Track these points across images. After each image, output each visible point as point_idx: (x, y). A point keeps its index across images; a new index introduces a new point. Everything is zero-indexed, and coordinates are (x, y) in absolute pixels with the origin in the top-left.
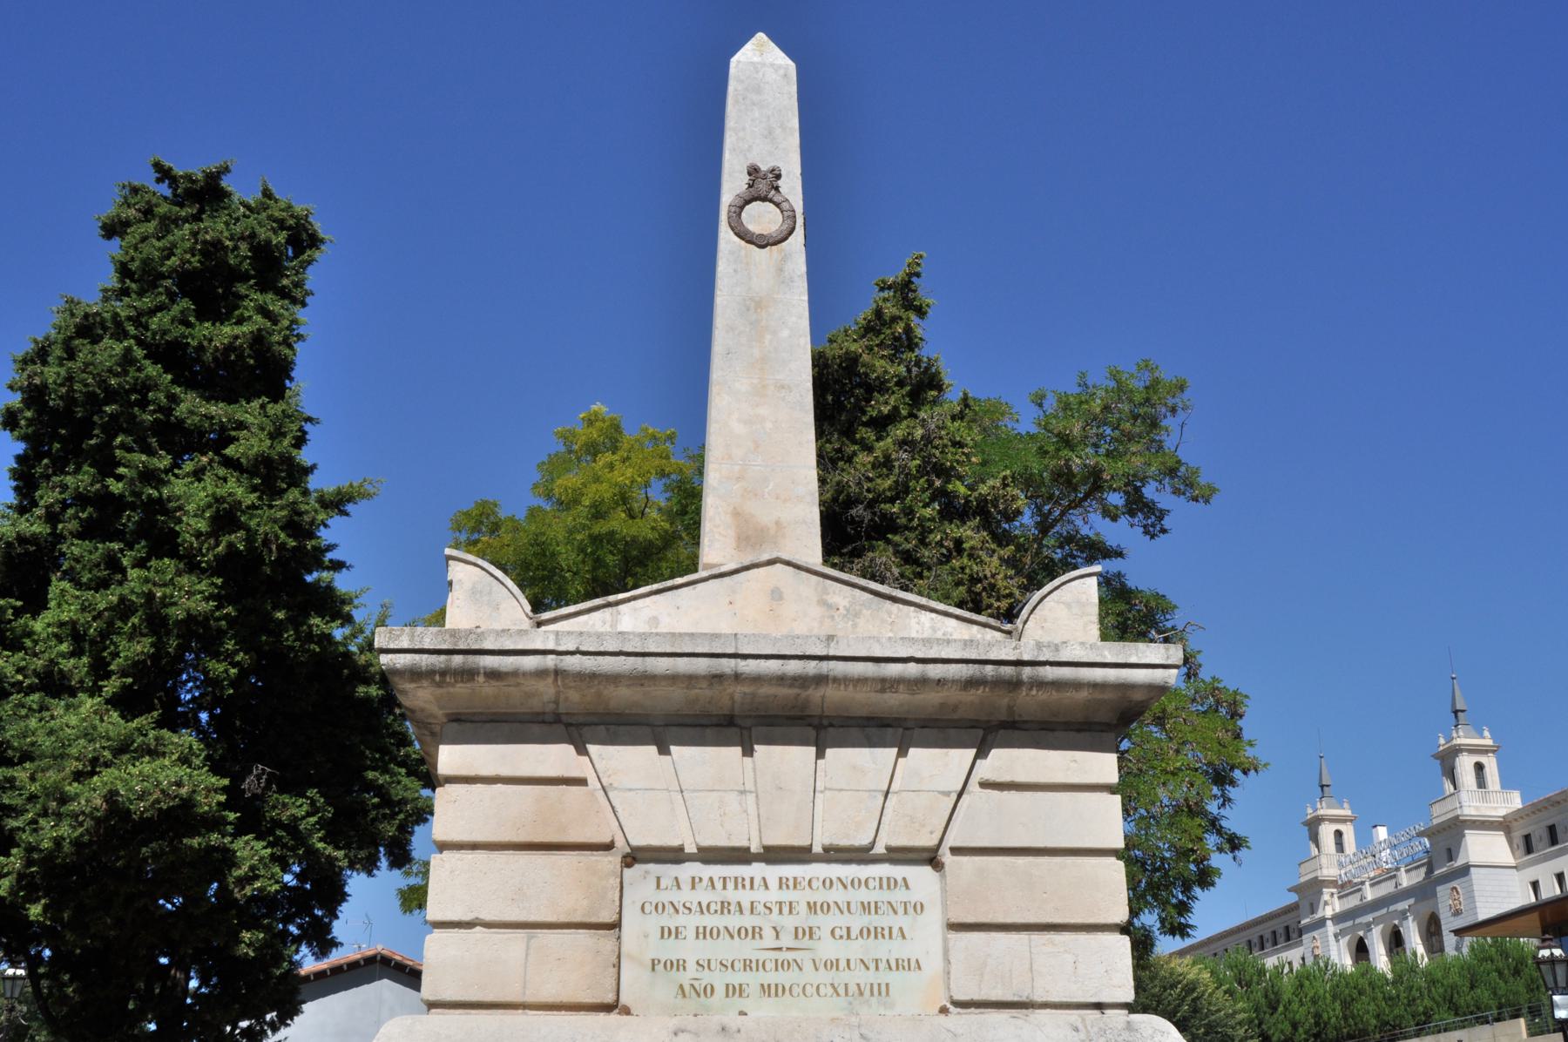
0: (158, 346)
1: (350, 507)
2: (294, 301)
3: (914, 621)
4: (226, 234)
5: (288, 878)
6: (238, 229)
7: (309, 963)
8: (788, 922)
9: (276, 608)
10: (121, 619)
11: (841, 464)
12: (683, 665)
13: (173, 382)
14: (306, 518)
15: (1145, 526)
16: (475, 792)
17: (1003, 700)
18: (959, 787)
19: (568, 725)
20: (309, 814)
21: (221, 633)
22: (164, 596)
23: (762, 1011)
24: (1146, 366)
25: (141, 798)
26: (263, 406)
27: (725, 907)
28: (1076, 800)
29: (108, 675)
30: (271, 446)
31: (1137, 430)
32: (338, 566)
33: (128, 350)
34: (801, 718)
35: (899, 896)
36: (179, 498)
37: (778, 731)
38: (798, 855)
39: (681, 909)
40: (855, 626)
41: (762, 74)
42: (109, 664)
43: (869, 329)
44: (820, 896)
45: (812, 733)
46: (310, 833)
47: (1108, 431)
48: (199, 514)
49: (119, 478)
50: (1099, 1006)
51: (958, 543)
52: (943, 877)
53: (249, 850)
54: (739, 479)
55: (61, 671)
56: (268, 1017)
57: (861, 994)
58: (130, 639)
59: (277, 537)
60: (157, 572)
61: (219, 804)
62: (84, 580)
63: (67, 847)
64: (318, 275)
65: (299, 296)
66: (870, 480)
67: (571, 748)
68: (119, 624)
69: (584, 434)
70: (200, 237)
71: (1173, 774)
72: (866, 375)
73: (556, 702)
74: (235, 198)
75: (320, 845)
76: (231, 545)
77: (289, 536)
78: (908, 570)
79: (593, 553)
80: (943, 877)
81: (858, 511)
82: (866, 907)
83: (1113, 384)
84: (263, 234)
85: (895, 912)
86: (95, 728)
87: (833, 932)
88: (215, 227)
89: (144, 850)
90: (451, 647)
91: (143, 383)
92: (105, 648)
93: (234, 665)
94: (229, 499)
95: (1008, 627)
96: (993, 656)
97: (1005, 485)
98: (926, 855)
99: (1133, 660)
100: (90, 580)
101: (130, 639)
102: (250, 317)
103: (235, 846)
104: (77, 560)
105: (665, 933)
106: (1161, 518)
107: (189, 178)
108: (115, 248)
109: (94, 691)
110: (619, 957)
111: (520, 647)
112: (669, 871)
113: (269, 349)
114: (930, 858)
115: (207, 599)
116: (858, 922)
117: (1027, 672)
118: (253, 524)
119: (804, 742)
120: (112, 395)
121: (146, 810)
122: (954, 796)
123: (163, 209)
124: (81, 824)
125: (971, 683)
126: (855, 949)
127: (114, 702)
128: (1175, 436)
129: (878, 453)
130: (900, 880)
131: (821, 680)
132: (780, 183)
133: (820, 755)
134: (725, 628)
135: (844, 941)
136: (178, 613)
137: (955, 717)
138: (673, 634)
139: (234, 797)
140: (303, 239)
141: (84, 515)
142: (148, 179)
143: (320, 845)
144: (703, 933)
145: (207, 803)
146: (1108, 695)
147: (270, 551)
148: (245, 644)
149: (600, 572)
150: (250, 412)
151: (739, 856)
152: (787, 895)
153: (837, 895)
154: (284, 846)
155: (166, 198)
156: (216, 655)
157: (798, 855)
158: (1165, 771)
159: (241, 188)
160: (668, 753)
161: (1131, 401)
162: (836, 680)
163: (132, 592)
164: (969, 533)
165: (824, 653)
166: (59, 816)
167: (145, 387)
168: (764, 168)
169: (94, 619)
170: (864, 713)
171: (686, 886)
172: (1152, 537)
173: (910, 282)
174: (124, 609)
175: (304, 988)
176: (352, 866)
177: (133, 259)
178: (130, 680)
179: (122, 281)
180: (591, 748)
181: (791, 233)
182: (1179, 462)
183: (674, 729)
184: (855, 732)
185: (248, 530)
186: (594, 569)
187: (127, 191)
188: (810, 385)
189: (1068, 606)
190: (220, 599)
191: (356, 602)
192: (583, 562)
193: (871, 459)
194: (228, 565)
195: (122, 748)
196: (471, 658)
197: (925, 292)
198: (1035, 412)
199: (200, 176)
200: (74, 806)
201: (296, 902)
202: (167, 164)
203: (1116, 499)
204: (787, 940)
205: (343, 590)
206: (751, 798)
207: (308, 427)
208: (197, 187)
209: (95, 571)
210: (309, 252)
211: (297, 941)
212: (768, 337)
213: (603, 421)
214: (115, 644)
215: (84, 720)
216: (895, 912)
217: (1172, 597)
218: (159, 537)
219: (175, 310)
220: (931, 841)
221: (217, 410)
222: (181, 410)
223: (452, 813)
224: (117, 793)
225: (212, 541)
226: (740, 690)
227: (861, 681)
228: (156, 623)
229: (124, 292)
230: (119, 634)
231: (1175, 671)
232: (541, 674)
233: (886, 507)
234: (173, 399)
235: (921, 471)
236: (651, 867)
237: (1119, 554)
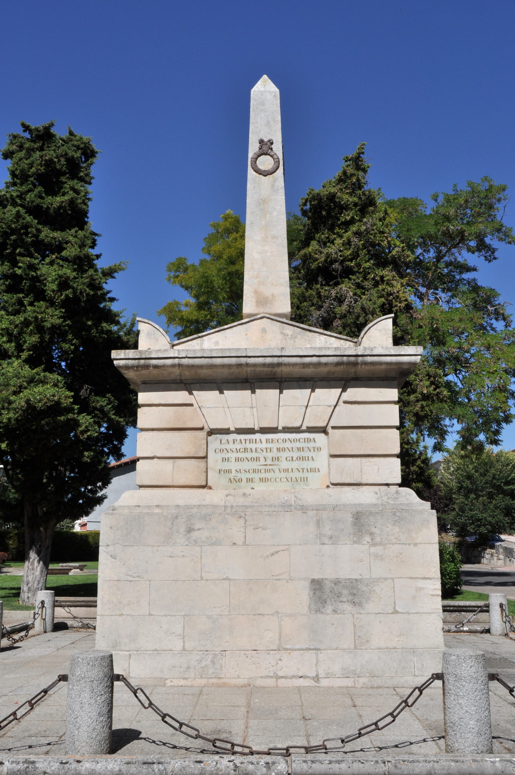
0: (31, 207)
1: (115, 275)
2: (86, 182)
3: (318, 339)
4: (54, 155)
5: (103, 429)
6: (59, 152)
7: (112, 462)
8: (270, 455)
9: (88, 320)
10: (26, 327)
11: (328, 244)
12: (226, 361)
13: (38, 223)
14: (97, 282)
15: (485, 257)
16: (153, 408)
17: (352, 370)
18: (335, 404)
19: (185, 384)
20: (108, 404)
21: (66, 332)
22: (42, 318)
23: (260, 487)
24: (486, 179)
25: (39, 402)
26: (76, 232)
27: (246, 450)
28: (382, 405)
29: (23, 351)
30: (80, 251)
31: (482, 211)
32: (112, 300)
33: (18, 212)
34: (274, 378)
35: (311, 445)
36: (44, 275)
37: (264, 384)
38: (273, 430)
39: (229, 451)
40: (295, 342)
41: (265, 93)
42: (23, 346)
43: (340, 181)
44: (281, 445)
45: (278, 384)
46: (109, 412)
47: (469, 211)
48: (53, 281)
49: (20, 268)
50: (387, 485)
51: (382, 277)
52: (328, 437)
53: (85, 420)
54: (257, 277)
55: (4, 348)
56: (98, 485)
57: (297, 481)
58: (30, 336)
59: (86, 291)
60: (38, 307)
61: (70, 402)
62: (10, 310)
63: (13, 422)
64: (97, 169)
65: (88, 180)
66: (341, 251)
67: (187, 393)
68: (25, 329)
69: (224, 225)
70: (44, 158)
71: (493, 373)
72: (340, 202)
73: (181, 376)
74: (58, 137)
75: (113, 417)
76: (67, 296)
77: (90, 290)
78: (359, 292)
79: (229, 280)
80: (328, 437)
81: (336, 266)
82: (299, 449)
83: (470, 189)
84: (70, 153)
85: (310, 451)
86: (19, 373)
87: (286, 459)
88: (50, 154)
89: (43, 422)
90: (139, 357)
91: (26, 225)
92: (21, 339)
93: (72, 345)
94: (64, 276)
95: (355, 340)
96: (346, 354)
97: (403, 251)
98: (322, 430)
99: (403, 353)
100: (12, 310)
101: (30, 336)
102: (68, 192)
103: (79, 418)
104: (6, 302)
105: (224, 460)
106: (493, 253)
107: (37, 129)
108: (9, 163)
109: (18, 357)
110: (207, 469)
111: (165, 356)
112: (224, 437)
113: (77, 206)
114: (324, 430)
115: (59, 318)
116: (296, 455)
117: (360, 359)
118: (75, 285)
119: (274, 388)
120: (13, 231)
121: (42, 406)
122: (333, 407)
123: (27, 145)
124: (17, 412)
125: (338, 364)
126: (295, 465)
127: (27, 361)
128: (501, 212)
129: (345, 239)
130: (312, 439)
131: (279, 365)
132: (273, 146)
133: (281, 392)
134: (244, 346)
135: (290, 462)
136: (48, 325)
137: (334, 376)
138: (222, 349)
139: (77, 399)
140: (89, 153)
141: (7, 283)
142: (19, 131)
143: (113, 417)
144: (237, 460)
145: (66, 402)
146: (393, 367)
147: (83, 296)
148: (76, 336)
149: (234, 288)
150: (70, 235)
151: (251, 431)
152: (269, 445)
153: (288, 445)
154: (99, 417)
155: (28, 139)
156: (65, 341)
157: (273, 430)
158: (489, 372)
159: (60, 132)
160: (223, 393)
161: (478, 196)
162: (285, 365)
163: (29, 316)
164: (387, 273)
165: (280, 355)
166: (8, 409)
167: (26, 227)
168: (266, 140)
169: (15, 328)
170: (298, 376)
171: (231, 442)
172: (490, 261)
173: (359, 157)
174: (26, 323)
175: (112, 473)
176: (127, 424)
177: (16, 170)
178: (32, 352)
179: (13, 179)
180: (194, 392)
181: (278, 168)
182: (502, 225)
183: (225, 384)
184: (295, 383)
185: (73, 288)
186: (230, 287)
187: (11, 137)
188: (286, 236)
189: (380, 331)
190: (64, 318)
191: (121, 315)
192: (226, 283)
193: (341, 241)
194: (66, 303)
195: (31, 381)
196: (147, 361)
197: (367, 160)
198: (433, 204)
199: (41, 128)
200: (14, 406)
201: (106, 438)
202: (27, 124)
203: (473, 244)
204: (269, 462)
205: (115, 311)
206: (255, 410)
207: (96, 238)
208: (41, 133)
209: (14, 307)
210: (91, 160)
211: (108, 454)
212: (268, 215)
213: (232, 218)
214: (24, 338)
215: (15, 370)
216: (310, 451)
217: (498, 290)
218: (39, 295)
219: (37, 191)
220: (323, 424)
221: (57, 234)
222: (42, 236)
223: (145, 417)
224: (30, 400)
225: (59, 294)
226: (249, 369)
227: (295, 365)
228: (40, 329)
229: (14, 184)
230: (25, 333)
231: (420, 357)
232: (173, 366)
233: (348, 263)
234: (39, 231)
235: (364, 246)
236: (218, 436)
237: (475, 269)
